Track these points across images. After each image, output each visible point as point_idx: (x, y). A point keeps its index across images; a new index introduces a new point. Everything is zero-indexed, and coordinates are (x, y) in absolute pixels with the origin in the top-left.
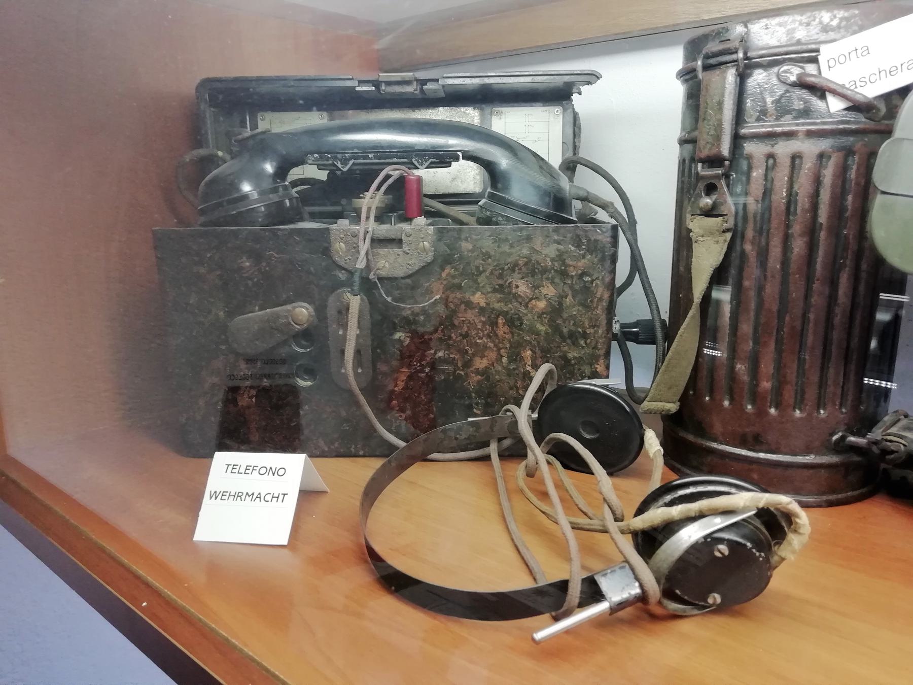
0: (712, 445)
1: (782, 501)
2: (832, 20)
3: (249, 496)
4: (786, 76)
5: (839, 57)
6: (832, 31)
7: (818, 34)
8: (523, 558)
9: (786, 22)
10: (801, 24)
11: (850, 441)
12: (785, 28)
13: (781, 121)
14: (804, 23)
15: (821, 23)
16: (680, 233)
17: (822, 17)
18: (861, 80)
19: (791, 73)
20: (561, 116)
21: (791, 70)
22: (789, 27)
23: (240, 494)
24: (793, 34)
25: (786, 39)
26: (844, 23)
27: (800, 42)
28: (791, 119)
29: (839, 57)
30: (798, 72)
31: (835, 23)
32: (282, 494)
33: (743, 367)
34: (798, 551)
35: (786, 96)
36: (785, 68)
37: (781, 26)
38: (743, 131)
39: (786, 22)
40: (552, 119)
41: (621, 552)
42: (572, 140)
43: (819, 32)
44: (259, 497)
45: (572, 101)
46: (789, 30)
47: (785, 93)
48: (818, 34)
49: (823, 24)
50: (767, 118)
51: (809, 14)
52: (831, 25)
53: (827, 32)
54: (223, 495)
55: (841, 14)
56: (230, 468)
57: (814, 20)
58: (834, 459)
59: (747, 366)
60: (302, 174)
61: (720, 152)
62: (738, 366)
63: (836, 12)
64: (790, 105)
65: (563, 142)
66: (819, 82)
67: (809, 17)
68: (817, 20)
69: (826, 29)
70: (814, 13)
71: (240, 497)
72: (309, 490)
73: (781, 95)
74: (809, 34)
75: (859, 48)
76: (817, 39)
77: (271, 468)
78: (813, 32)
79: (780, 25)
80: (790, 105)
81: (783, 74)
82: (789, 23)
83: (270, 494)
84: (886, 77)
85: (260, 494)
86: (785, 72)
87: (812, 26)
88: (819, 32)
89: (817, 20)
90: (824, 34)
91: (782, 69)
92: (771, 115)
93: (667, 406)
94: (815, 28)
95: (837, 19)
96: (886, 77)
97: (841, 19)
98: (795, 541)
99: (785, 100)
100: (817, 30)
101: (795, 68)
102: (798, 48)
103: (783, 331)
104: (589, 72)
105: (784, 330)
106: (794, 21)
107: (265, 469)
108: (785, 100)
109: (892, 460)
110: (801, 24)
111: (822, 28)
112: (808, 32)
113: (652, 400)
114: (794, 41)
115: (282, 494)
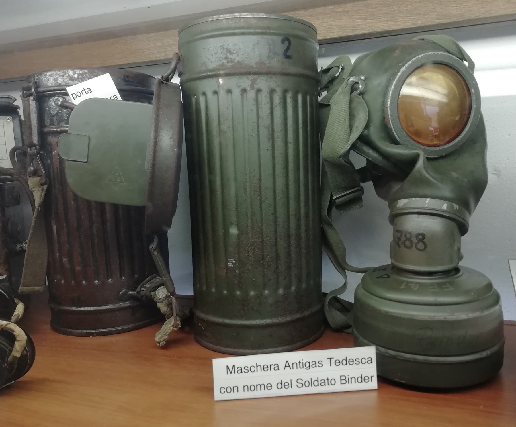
0: (73, 309)
1: (2, 324)
2: (74, 75)
4: (57, 102)
6: (75, 80)
7: (68, 81)
9: (53, 74)
10: (60, 76)
11: (130, 294)
12: (53, 77)
13: (60, 125)
14: (61, 75)
15: (69, 75)
17: (69, 73)
19: (59, 100)
20: (12, 122)
21: (59, 99)
22: (55, 77)
24: (57, 81)
25: (54, 83)
26: (80, 76)
27: (60, 85)
28: (64, 124)
30: (62, 100)
31: (76, 76)
33: (66, 260)
34: (19, 350)
35: (60, 112)
36: (56, 98)
37: (51, 76)
38: (46, 130)
39: (53, 74)
40: (5, 124)
42: (21, 137)
43: (69, 80)
45: (19, 113)
46: (55, 78)
47: (59, 111)
48: (68, 81)
49: (70, 76)
50: (53, 123)
51: (62, 71)
52: (74, 77)
53: (73, 80)
55: (78, 72)
57: (66, 74)
58: (127, 304)
59: (68, 259)
61: (32, 142)
62: (64, 260)
63: (75, 71)
64: (62, 117)
65: (15, 138)
66: (68, 105)
67: (63, 73)
68: (67, 74)
69: (72, 79)
70: (65, 71)
73: (58, 112)
74: (65, 81)
75: (86, 89)
76: (69, 84)
78: (66, 80)
79: (51, 75)
80: (62, 117)
81: (56, 101)
82: (54, 75)
86: (57, 100)
87: (65, 77)
88: (69, 80)
89: (67, 74)
90: (72, 81)
91: (55, 98)
92: (55, 122)
93: (36, 289)
94: (67, 78)
95: (76, 74)
97: (79, 74)
98: (17, 345)
99: (60, 114)
100: (68, 79)
101: (61, 98)
102: (59, 88)
103: (81, 238)
104: (7, 96)
105: (82, 237)
106: (56, 74)
108: (60, 114)
110: (60, 76)
111: (70, 78)
112: (64, 80)
113: (23, 286)
114: (58, 84)
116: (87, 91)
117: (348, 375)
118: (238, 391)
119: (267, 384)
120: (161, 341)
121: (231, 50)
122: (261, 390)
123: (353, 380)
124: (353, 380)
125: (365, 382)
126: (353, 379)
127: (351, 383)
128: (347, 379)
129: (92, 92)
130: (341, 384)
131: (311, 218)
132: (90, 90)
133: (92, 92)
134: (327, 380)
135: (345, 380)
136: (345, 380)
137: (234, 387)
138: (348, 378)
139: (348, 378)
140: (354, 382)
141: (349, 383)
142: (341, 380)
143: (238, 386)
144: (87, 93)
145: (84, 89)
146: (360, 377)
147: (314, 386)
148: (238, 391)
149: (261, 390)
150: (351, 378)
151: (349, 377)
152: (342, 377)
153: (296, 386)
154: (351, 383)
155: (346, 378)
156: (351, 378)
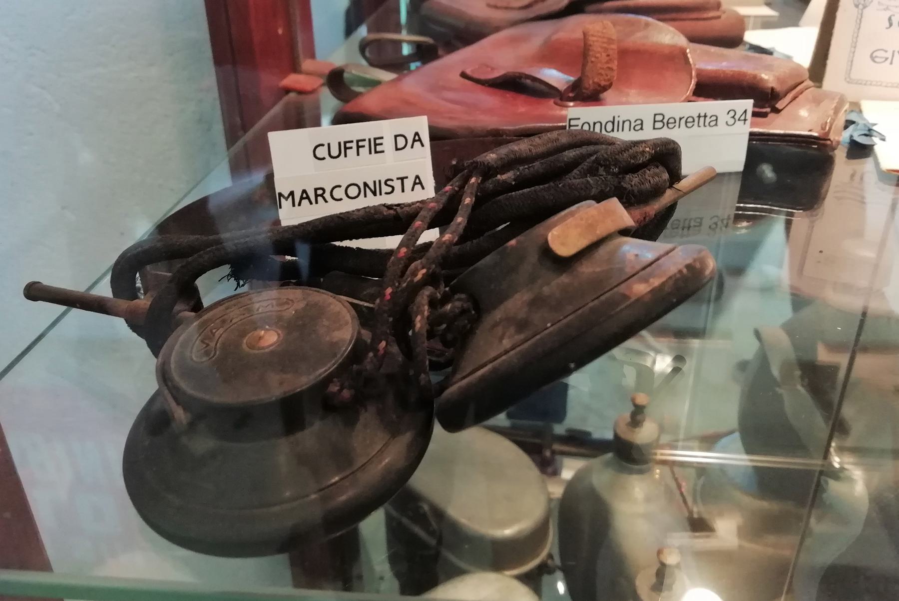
3: (287, 199)
5: (730, 111)
8: (787, 105)
16: (856, 83)
18: (389, 183)
23: (320, 192)
29: (730, 111)
32: (398, 179)
41: (784, 108)
44: (305, 195)
54: (376, 145)
56: (683, 121)
60: (656, 127)
71: (322, 195)
72: (10, 370)
75: (709, 115)
77: (366, 185)
83: (323, 145)
84: (630, 130)
85: (417, 134)
96: (630, 130)
107: (356, 188)
109: (192, 323)
115: (398, 179)
116: (708, 120)
117: (619, 117)
118: (679, 127)
119: (670, 119)
120: (603, 83)
121: (825, 146)
122: (403, 191)
123: (627, 124)
124: (627, 124)
125: (668, 127)
126: (627, 124)
127: (623, 130)
128: (665, 121)
129: (732, 117)
130: (654, 128)
131: (808, 139)
132: (642, 124)
133: (732, 117)
134: (698, 117)
135: (662, 121)
136: (662, 121)
137: (595, 124)
138: (618, 122)
139: (618, 122)
140: (628, 129)
141: (380, 181)
142: (655, 121)
143: (601, 121)
144: (707, 124)
145: (705, 114)
146: (611, 121)
147: (359, 185)
148: (679, 127)
149: (403, 191)
150: (624, 122)
151: (619, 119)
152: (571, 121)
153: (391, 178)
154: (623, 130)
155: (663, 118)
156: (624, 122)
